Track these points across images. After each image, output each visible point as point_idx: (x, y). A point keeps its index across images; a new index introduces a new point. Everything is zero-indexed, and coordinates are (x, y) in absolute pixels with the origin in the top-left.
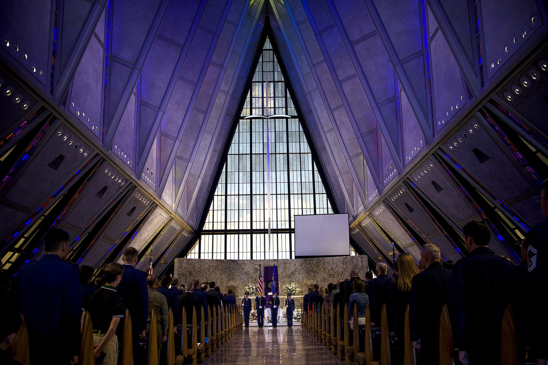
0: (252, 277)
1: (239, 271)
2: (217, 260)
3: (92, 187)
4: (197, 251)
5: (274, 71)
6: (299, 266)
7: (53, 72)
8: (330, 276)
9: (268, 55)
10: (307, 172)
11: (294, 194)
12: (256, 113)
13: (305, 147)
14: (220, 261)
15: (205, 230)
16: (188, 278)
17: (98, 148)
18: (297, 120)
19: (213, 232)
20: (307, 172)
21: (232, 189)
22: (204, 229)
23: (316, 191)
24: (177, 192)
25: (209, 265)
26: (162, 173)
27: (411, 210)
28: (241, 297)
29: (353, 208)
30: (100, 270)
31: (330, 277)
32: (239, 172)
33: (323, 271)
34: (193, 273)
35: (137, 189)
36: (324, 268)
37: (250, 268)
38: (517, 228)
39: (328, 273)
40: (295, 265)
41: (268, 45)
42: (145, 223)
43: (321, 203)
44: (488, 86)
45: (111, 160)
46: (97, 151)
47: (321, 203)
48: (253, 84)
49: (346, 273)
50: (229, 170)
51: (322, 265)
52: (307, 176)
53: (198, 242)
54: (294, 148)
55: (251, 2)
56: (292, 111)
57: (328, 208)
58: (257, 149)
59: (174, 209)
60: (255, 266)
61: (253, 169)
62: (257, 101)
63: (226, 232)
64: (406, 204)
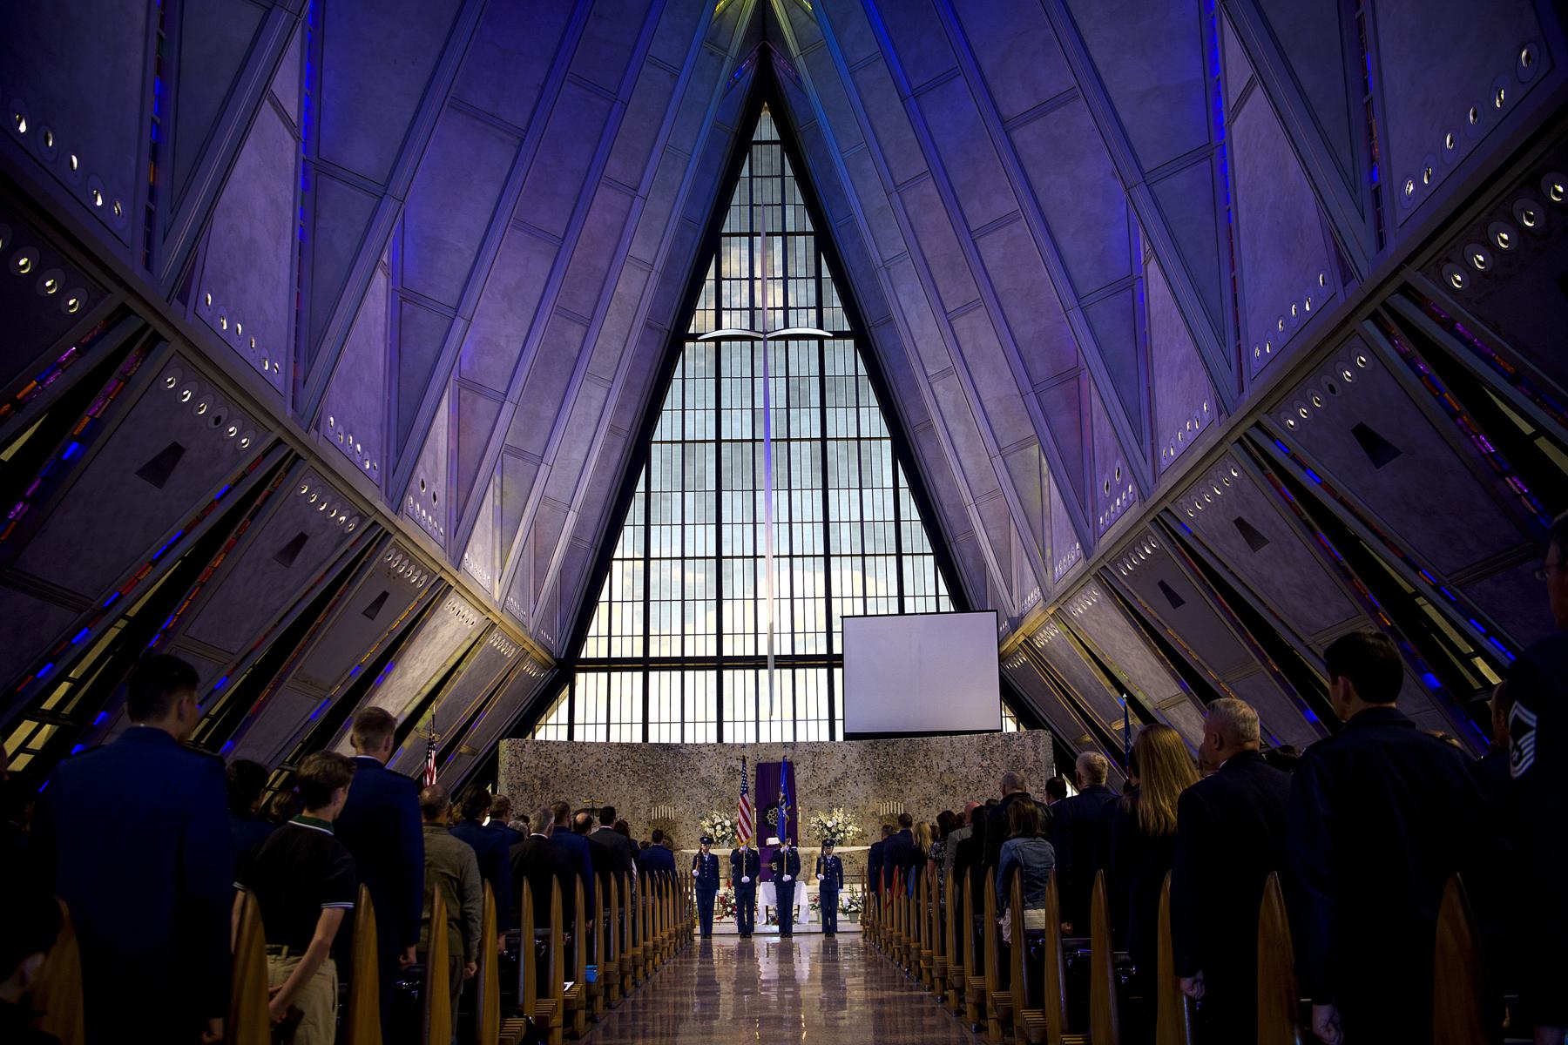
0: (721, 794)
1: (685, 775)
2: (620, 745)
3: (264, 537)
4: (564, 718)
5: (783, 204)
6: (856, 762)
7: (153, 207)
8: (945, 789)
9: (767, 158)
10: (878, 493)
11: (841, 556)
12: (733, 323)
13: (874, 422)
14: (630, 746)
15: (586, 659)
16: (539, 796)
17: (279, 424)
18: (850, 343)
19: (610, 665)
20: (878, 493)
21: (665, 542)
22: (583, 656)
23: (905, 548)
24: (505, 549)
25: (598, 760)
26: (463, 496)
27: (1176, 601)
28: (688, 851)
29: (1011, 595)
30: (286, 773)
31: (944, 792)
32: (683, 492)
33: (925, 775)
34: (552, 782)
35: (393, 540)
36: (926, 767)
37: (716, 766)
38: (1481, 651)
39: (939, 782)
40: (844, 757)
41: (766, 128)
42: (414, 639)
43: (919, 580)
44: (1397, 246)
45: (319, 459)
46: (277, 433)
47: (919, 580)
48: (724, 240)
49: (991, 781)
50: (655, 487)
51: (921, 758)
52: (878, 503)
53: (566, 692)
54: (841, 423)
55: (718, 7)
56: (837, 317)
57: (937, 596)
58: (737, 425)
59: (497, 597)
60: (729, 762)
61: (725, 484)
62: (736, 291)
63: (646, 664)
64: (1162, 585)
